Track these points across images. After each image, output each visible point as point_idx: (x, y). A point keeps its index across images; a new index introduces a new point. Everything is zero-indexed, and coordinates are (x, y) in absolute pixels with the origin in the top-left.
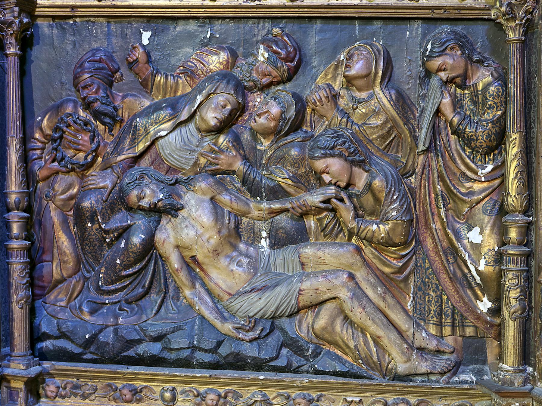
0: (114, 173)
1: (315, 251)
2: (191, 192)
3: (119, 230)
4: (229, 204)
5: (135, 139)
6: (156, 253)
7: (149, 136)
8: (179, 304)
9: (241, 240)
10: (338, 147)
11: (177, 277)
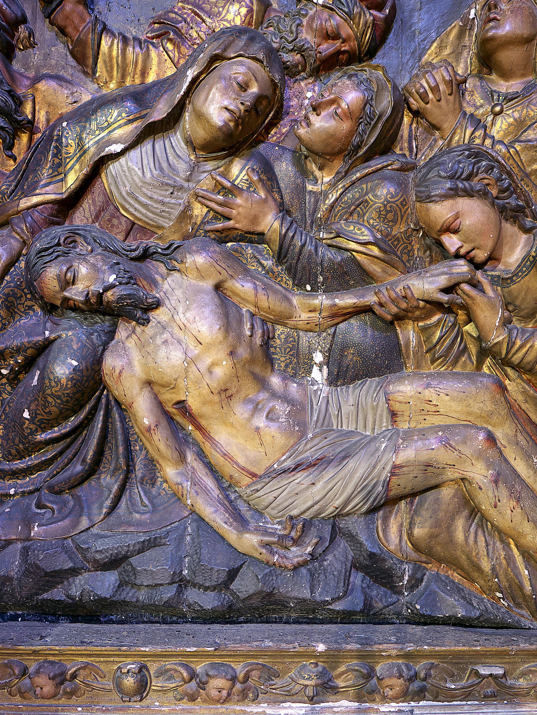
0: (14, 234)
1: (420, 390)
2: (176, 275)
3: (25, 351)
4: (252, 298)
5: (60, 165)
6: (107, 396)
7: (88, 156)
8: (154, 491)
9: (273, 370)
10: (480, 176)
11: (150, 443)
